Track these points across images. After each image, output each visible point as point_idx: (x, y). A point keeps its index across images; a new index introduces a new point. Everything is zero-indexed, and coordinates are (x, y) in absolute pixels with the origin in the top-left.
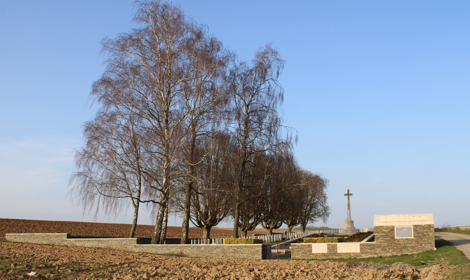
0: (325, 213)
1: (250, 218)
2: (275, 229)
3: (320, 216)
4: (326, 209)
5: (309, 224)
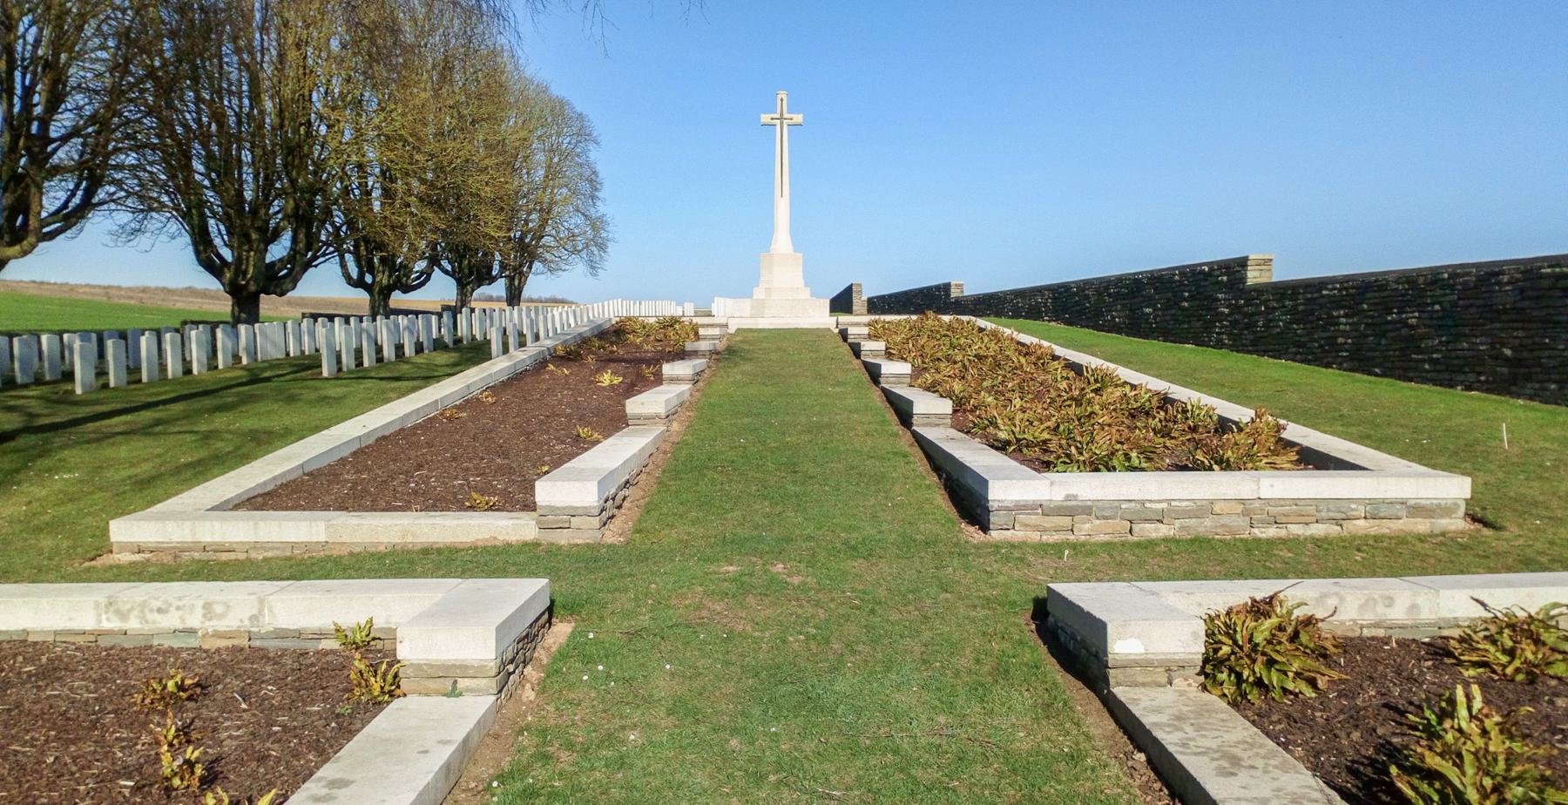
0: (593, 244)
1: (276, 235)
3: (575, 251)
4: (597, 224)
5: (537, 284)
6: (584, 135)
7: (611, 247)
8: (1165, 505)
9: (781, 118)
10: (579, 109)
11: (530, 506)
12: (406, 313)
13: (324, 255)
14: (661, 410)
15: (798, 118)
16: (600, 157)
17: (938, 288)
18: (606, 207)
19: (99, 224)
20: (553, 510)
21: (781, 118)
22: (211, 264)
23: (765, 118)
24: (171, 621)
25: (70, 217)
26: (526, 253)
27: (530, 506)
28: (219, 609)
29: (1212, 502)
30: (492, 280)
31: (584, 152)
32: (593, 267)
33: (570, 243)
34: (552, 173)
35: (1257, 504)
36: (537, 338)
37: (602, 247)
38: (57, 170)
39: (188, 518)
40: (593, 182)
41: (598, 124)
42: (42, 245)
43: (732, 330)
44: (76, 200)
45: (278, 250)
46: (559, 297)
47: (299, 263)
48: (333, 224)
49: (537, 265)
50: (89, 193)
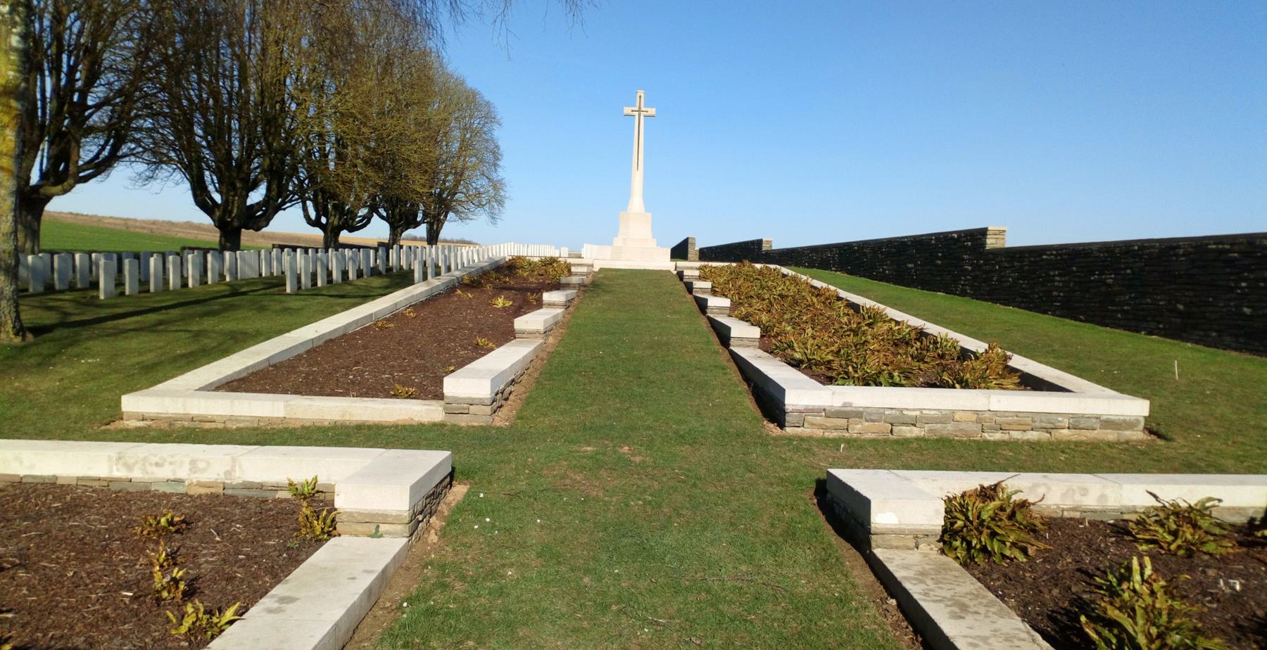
0: (493, 199)
1: (254, 186)
2: (350, 231)
3: (480, 205)
4: (497, 186)
5: (451, 229)
6: (490, 117)
7: (507, 203)
8: (917, 413)
9: (639, 111)
10: (487, 98)
11: (439, 396)
12: (351, 247)
13: (291, 201)
14: (541, 328)
15: (652, 111)
16: (502, 136)
17: (753, 243)
18: (507, 171)
19: (122, 172)
20: (457, 400)
21: (639, 111)
22: (202, 200)
23: (627, 110)
24: (165, 473)
25: (100, 166)
26: (440, 209)
27: (439, 396)
28: (201, 465)
29: (953, 412)
30: (417, 224)
31: (490, 130)
32: (493, 217)
33: (477, 200)
34: (465, 146)
35: (987, 415)
36: (449, 269)
37: (500, 203)
38: (92, 130)
39: (183, 395)
40: (496, 154)
41: (502, 109)
42: (79, 186)
43: (596, 269)
44: (106, 153)
45: (256, 196)
46: (467, 239)
47: (272, 206)
48: (298, 178)
49: (451, 215)
50: (115, 148)
